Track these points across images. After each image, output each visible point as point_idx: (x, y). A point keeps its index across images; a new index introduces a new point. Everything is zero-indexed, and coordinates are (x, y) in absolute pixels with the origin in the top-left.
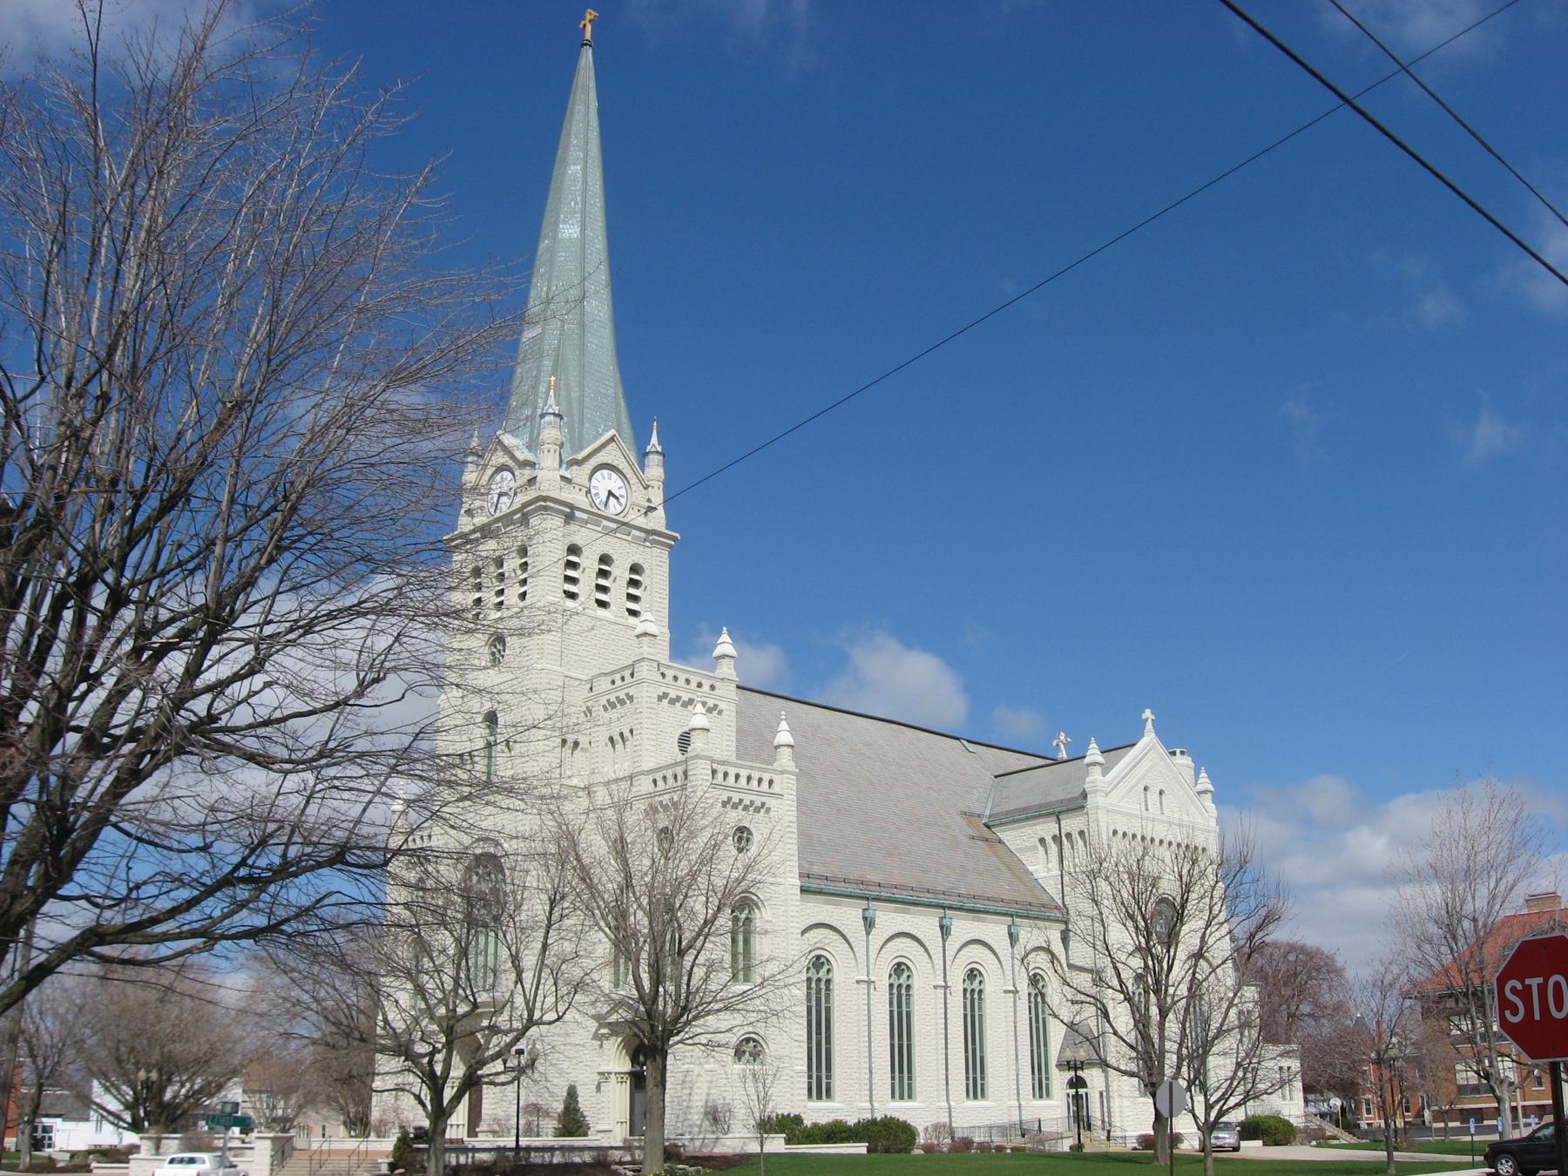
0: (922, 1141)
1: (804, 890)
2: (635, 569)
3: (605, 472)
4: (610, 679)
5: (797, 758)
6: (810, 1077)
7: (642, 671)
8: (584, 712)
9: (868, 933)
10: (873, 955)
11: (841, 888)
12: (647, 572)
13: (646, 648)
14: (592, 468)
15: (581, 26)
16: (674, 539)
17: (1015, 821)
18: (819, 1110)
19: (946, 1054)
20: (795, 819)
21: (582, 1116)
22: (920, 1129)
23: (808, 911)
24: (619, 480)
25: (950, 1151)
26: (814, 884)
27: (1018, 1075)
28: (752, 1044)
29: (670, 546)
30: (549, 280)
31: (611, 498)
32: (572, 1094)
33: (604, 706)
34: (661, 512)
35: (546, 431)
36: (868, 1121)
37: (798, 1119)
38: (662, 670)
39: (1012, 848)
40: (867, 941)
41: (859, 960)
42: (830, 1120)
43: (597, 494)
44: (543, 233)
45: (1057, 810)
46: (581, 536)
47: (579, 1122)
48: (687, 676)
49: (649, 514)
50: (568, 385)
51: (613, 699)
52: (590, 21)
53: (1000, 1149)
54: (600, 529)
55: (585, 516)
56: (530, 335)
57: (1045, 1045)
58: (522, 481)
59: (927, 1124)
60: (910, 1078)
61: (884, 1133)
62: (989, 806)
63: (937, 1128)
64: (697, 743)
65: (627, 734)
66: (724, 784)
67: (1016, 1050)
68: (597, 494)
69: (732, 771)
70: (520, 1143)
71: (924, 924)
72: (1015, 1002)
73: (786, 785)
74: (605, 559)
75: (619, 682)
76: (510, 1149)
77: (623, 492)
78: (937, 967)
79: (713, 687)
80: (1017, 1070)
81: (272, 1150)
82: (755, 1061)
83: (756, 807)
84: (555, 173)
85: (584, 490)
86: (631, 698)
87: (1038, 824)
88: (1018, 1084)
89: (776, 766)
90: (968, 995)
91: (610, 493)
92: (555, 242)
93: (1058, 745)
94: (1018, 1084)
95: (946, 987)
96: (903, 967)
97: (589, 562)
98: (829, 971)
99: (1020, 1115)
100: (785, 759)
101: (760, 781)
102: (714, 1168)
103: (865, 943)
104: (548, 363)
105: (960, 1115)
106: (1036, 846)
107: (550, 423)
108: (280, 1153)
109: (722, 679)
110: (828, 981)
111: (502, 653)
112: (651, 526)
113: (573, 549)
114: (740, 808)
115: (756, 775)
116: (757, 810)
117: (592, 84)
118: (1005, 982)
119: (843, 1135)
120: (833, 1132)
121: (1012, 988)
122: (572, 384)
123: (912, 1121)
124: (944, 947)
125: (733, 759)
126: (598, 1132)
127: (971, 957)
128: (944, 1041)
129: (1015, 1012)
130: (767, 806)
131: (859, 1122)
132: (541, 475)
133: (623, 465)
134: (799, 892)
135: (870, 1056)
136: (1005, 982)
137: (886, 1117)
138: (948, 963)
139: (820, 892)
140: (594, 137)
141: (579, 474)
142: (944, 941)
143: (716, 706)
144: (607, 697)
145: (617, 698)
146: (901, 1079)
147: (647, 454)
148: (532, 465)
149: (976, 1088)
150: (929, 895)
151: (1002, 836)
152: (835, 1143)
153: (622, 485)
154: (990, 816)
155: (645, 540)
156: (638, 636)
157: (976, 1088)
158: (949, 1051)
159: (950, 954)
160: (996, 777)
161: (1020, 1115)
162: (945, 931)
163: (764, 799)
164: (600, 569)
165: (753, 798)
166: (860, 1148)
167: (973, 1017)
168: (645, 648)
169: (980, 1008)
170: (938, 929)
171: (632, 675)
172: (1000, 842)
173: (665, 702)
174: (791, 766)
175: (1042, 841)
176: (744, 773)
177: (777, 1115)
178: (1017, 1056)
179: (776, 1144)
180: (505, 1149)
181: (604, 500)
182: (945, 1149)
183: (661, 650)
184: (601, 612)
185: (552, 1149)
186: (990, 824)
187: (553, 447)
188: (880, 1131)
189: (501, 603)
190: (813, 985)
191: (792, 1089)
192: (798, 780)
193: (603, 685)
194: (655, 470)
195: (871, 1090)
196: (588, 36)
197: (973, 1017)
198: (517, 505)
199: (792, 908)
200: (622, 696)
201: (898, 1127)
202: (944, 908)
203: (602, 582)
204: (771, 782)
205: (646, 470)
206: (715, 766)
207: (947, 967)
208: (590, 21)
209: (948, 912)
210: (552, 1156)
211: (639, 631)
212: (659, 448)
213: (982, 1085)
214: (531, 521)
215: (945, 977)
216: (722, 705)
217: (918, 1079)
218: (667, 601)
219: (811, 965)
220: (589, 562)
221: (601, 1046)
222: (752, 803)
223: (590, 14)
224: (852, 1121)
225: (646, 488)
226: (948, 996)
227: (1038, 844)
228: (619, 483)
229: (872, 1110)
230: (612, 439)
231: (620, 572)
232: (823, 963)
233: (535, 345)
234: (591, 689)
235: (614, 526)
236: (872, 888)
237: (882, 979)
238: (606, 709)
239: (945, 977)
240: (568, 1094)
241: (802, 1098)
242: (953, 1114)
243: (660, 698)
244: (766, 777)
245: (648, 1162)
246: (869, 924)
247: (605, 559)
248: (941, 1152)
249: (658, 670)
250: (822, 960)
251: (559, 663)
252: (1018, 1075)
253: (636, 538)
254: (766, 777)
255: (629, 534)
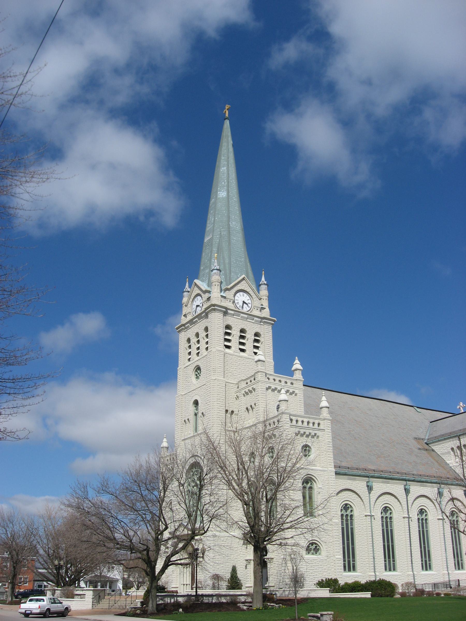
0: (400, 591)
1: (337, 473)
2: (257, 334)
3: (241, 293)
4: (245, 382)
5: (330, 413)
6: (344, 561)
7: (258, 377)
8: (236, 398)
9: (370, 493)
10: (372, 503)
11: (356, 472)
12: (262, 336)
13: (260, 367)
14: (235, 292)
15: (224, 112)
16: (274, 321)
17: (439, 441)
18: (349, 576)
19: (411, 549)
20: (331, 441)
21: (239, 580)
22: (399, 585)
23: (340, 483)
24: (248, 296)
25: (414, 596)
26: (343, 471)
27: (447, 559)
28: (314, 545)
29: (272, 324)
30: (214, 216)
31: (245, 304)
32: (234, 570)
33: (243, 394)
34: (267, 310)
35: (214, 277)
36: (371, 581)
37: (336, 581)
38: (268, 376)
39: (439, 453)
40: (369, 497)
41: (366, 506)
42: (353, 581)
43: (238, 303)
44: (212, 197)
45: (458, 434)
46: (230, 320)
47: (237, 583)
48: (280, 379)
49: (262, 311)
50: (223, 258)
51: (247, 391)
52: (228, 109)
53: (438, 594)
54: (240, 318)
55: (233, 312)
56: (208, 239)
57: (460, 544)
58: (205, 299)
59: (403, 583)
60: (394, 561)
61: (379, 587)
62: (428, 435)
63: (408, 584)
64: (283, 407)
65: (253, 406)
66: (297, 425)
67: (445, 547)
68: (238, 303)
69: (300, 419)
70: (198, 593)
71: (397, 488)
72: (443, 524)
73: (326, 425)
74: (242, 331)
75: (249, 383)
76: (193, 596)
77: (250, 301)
78: (404, 508)
79: (292, 384)
80: (446, 556)
81: (93, 596)
82: (316, 553)
83: (307, 435)
84: (216, 172)
85: (232, 301)
86: (254, 389)
87: (450, 441)
88: (447, 563)
89: (321, 417)
90: (420, 521)
91: (244, 302)
92: (216, 200)
93: (460, 408)
94: (447, 563)
95: (409, 518)
96: (388, 508)
97: (235, 333)
98: (391, 513)
99: (449, 578)
100: (325, 413)
101: (314, 424)
102: (287, 605)
103: (368, 498)
104: (215, 249)
105: (419, 578)
106: (450, 452)
107: (215, 273)
108: (98, 596)
109: (296, 380)
110: (351, 516)
111: (200, 374)
112: (263, 316)
113: (228, 327)
114: (305, 436)
115: (311, 421)
116: (313, 437)
117: (230, 134)
118: (404, 513)
119: (359, 588)
120: (354, 587)
121: (442, 518)
122: (226, 257)
123: (393, 581)
124: (407, 498)
125: (302, 414)
126: (246, 587)
127: (421, 503)
128: (409, 543)
129: (444, 529)
130: (317, 435)
131: (367, 582)
132: (212, 295)
133: (249, 290)
134: (334, 474)
135: (373, 551)
136: (404, 513)
137: (380, 579)
138: (410, 506)
139: (345, 474)
140: (232, 156)
141: (229, 295)
142: (407, 496)
143: (294, 392)
144: (245, 390)
145: (249, 390)
146: (389, 562)
147: (260, 285)
148: (209, 292)
149: (427, 565)
150: (398, 475)
151: (434, 448)
152: (355, 592)
153: (249, 298)
154: (428, 439)
155: (261, 322)
156: (256, 362)
157: (427, 565)
158: (412, 548)
159: (410, 502)
160: (431, 422)
161: (449, 578)
162: (407, 491)
163: (316, 432)
164: (240, 335)
165: (311, 431)
166: (367, 595)
167: (423, 531)
168: (260, 367)
169: (427, 527)
170: (404, 490)
171: (255, 379)
172: (433, 450)
173: (270, 390)
174: (328, 416)
175: (452, 449)
176: (306, 420)
177: (326, 579)
178: (446, 550)
179: (325, 593)
180: (191, 596)
181: (241, 305)
182: (412, 595)
183: (270, 369)
184: (242, 354)
185: (212, 596)
186: (428, 443)
187: (217, 283)
188: (377, 586)
189: (199, 353)
190: (344, 518)
191: (335, 566)
192: (331, 423)
193: (243, 385)
194: (264, 292)
195: (374, 566)
196: (227, 115)
197: (423, 531)
198: (203, 310)
199: (331, 482)
200: (251, 389)
201: (386, 584)
202: (406, 480)
203: (242, 341)
204: (319, 424)
205: (260, 292)
206: (291, 417)
207: (409, 508)
208: (228, 109)
209: (408, 482)
210: (212, 599)
211: (256, 359)
212: (265, 282)
213: (430, 564)
214: (209, 315)
215: (408, 513)
216: (297, 391)
217: (398, 561)
218: (272, 348)
219: (343, 508)
220: (235, 333)
221: (247, 548)
222: (310, 433)
223: (227, 107)
224: (363, 581)
225: (260, 299)
226: (410, 522)
227: (451, 451)
228: (248, 298)
229: (375, 576)
230: (243, 279)
231: (250, 336)
232: (348, 507)
233: (209, 243)
234: (238, 387)
235: (246, 316)
236: (370, 472)
237: (378, 514)
238: (244, 396)
239: (408, 513)
240: (232, 570)
241: (341, 571)
242: (415, 578)
243: (267, 389)
244: (317, 422)
245: (255, 601)
246: (370, 489)
247: (242, 331)
248: (410, 596)
249: (266, 376)
250: (348, 506)
251: (223, 376)
252: (447, 559)
253: (256, 321)
254: (317, 422)
255: (253, 320)
